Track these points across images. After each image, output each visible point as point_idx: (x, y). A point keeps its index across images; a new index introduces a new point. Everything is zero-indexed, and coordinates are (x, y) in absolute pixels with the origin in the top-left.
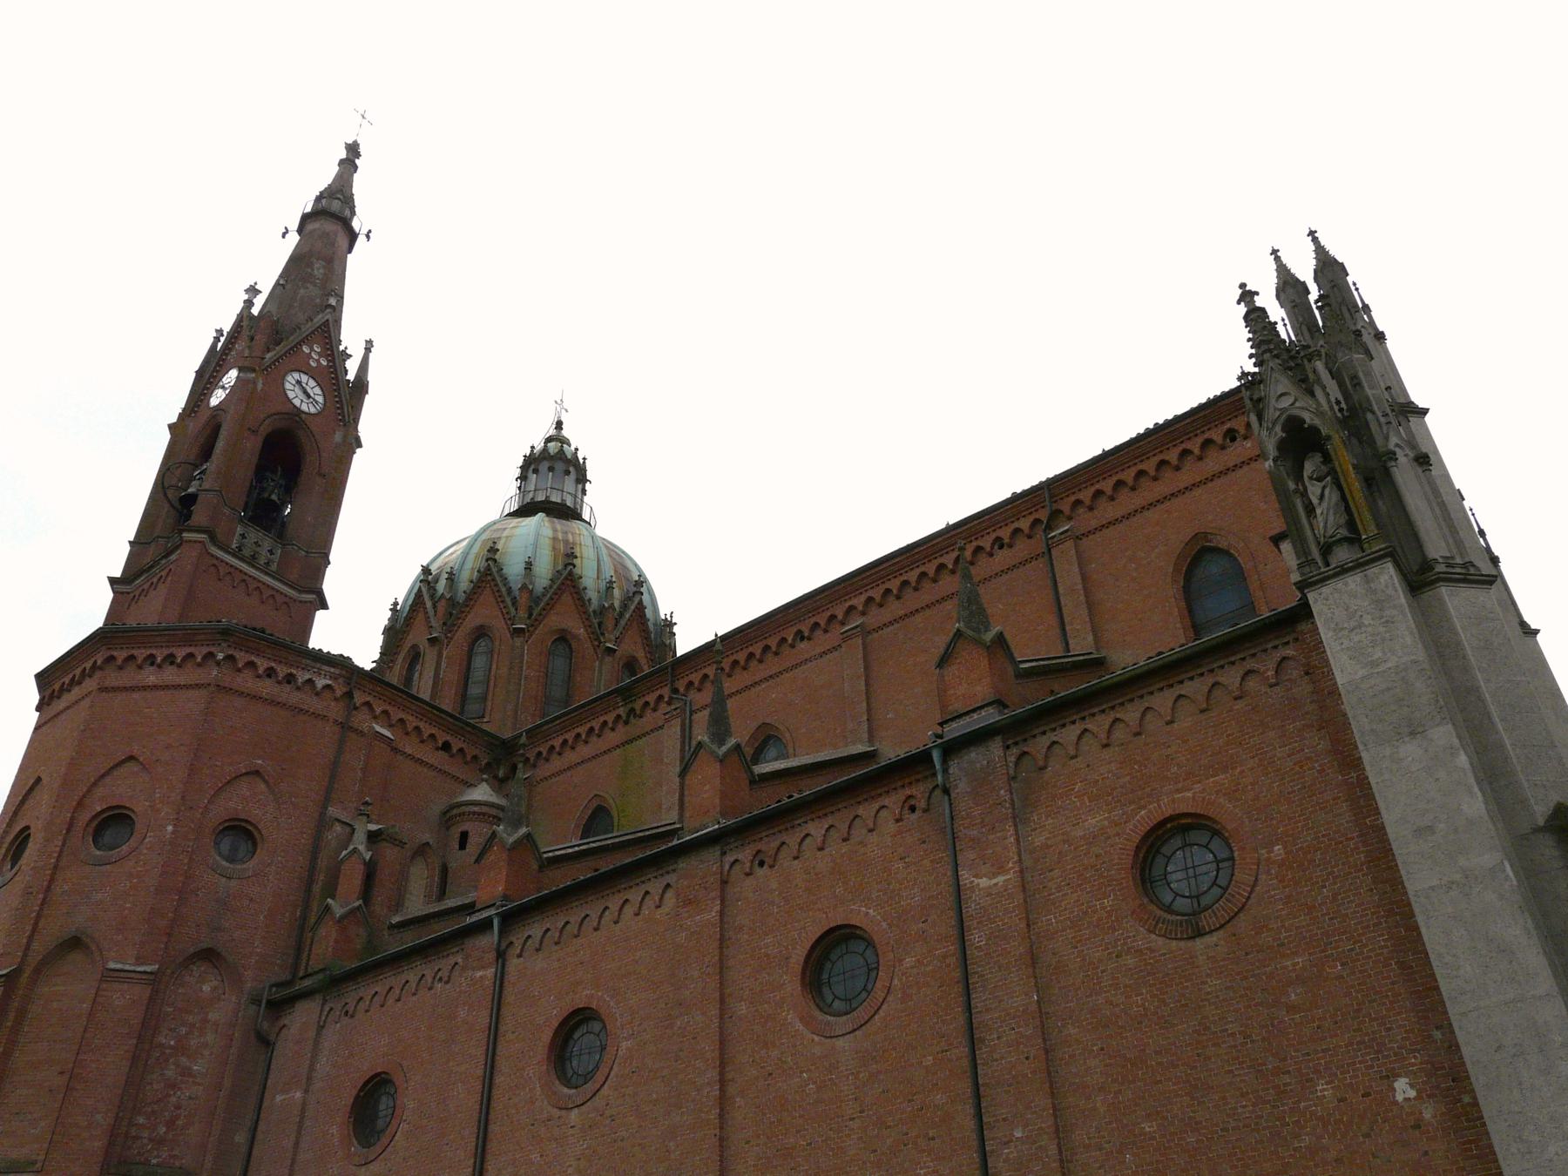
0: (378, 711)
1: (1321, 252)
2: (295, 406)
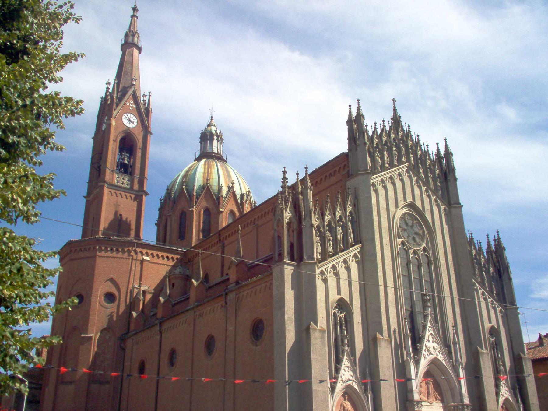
0: (144, 252)
2: (127, 127)
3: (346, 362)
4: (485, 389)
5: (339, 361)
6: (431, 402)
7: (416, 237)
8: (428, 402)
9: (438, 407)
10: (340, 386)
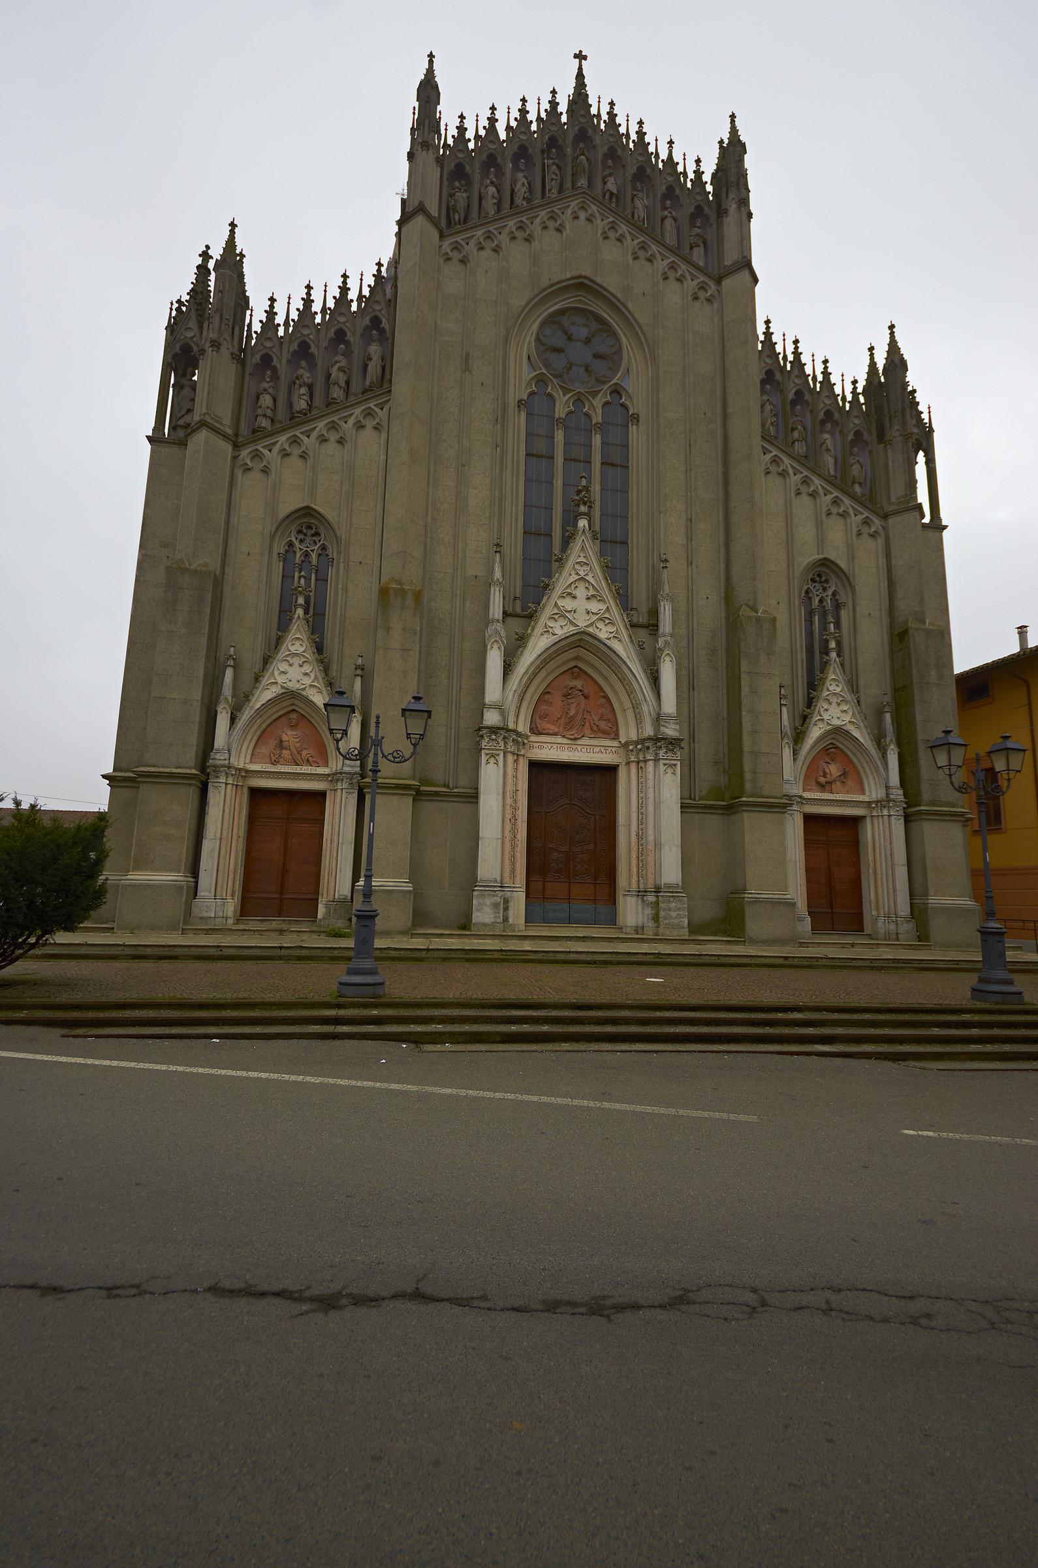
3: (834, 684)
5: (813, 685)
6: (572, 737)
8: (564, 736)
9: (596, 749)
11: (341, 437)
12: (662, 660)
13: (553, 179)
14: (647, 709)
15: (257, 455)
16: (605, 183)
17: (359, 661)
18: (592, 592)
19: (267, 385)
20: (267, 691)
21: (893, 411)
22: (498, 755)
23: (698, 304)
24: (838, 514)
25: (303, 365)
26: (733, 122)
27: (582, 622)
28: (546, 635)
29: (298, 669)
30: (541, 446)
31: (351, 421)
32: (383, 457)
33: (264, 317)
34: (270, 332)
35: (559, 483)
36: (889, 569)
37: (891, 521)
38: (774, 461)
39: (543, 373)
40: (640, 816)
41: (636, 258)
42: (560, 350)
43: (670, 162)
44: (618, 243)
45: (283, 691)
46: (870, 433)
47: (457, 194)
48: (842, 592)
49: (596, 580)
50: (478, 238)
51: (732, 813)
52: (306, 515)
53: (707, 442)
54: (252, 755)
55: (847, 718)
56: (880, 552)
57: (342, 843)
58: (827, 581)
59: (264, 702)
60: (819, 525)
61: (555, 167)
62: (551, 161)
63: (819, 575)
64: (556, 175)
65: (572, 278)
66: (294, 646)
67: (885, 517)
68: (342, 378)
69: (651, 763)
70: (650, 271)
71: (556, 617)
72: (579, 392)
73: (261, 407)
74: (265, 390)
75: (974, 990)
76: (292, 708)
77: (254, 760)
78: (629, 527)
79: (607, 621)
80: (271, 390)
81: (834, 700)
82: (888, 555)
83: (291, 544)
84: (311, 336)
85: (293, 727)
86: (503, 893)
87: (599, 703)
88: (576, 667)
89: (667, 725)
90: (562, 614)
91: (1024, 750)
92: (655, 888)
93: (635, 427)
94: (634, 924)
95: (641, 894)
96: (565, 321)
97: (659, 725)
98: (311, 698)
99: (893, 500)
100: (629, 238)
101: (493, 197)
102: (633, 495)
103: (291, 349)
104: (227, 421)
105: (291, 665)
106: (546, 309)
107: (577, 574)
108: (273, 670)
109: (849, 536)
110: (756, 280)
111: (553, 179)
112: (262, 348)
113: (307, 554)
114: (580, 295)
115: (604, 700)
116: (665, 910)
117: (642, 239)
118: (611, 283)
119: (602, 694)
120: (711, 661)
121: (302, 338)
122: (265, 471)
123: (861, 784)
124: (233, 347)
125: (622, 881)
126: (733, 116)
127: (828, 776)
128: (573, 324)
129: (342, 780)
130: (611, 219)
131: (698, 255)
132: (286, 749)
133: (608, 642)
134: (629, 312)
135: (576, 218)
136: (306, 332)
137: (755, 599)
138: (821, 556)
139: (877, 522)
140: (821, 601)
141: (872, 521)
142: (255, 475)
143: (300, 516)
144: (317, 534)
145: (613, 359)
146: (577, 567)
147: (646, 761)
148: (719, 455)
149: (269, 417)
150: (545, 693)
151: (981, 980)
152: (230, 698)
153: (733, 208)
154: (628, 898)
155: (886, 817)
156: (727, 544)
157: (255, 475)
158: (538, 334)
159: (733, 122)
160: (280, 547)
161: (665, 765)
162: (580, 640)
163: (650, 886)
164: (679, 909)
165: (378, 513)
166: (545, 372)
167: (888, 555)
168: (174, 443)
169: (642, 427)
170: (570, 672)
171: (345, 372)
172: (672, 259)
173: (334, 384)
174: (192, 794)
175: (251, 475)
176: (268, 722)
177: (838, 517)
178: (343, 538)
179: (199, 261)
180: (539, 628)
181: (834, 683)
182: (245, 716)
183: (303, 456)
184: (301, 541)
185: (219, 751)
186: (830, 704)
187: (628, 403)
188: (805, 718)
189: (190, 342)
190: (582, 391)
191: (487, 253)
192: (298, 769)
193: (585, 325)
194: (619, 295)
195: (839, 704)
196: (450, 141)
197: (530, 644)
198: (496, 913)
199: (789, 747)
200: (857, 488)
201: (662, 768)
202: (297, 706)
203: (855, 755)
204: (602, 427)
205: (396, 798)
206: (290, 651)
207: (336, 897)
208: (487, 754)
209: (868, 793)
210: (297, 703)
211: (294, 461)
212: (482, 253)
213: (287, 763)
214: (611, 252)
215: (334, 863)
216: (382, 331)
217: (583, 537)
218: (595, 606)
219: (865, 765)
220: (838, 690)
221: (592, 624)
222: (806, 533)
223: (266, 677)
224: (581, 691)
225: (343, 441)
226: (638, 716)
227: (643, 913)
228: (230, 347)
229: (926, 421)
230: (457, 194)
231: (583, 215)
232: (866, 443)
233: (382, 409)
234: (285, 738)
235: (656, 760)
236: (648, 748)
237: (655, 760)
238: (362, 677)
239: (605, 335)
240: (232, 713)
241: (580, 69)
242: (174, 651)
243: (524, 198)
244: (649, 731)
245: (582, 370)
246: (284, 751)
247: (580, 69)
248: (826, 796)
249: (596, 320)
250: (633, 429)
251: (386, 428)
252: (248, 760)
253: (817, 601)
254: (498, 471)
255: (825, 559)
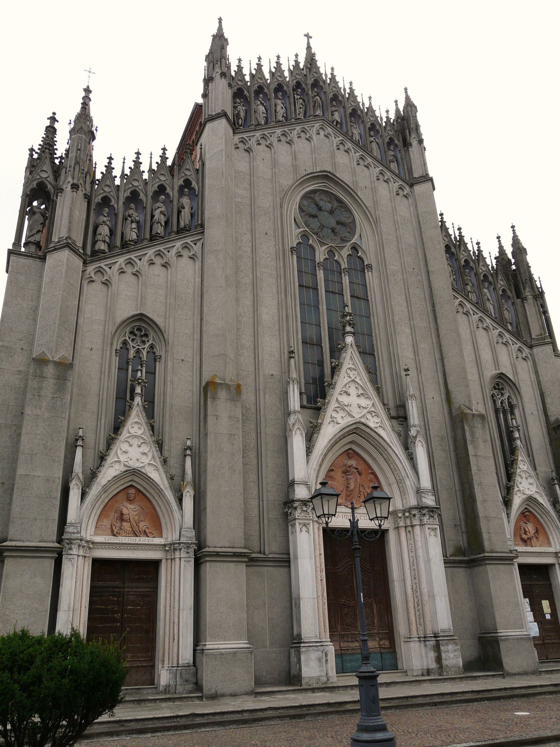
1: (408, 98)
4: (475, 478)
5: (117, 428)
7: (338, 227)
10: (517, 501)
11: (166, 262)
12: (294, 433)
13: (300, 108)
14: (409, 483)
15: (100, 271)
16: (333, 115)
17: (189, 443)
18: (361, 391)
19: (105, 219)
20: (110, 469)
21: (524, 279)
22: (308, 524)
23: (399, 198)
24: (502, 343)
25: (133, 207)
26: (406, 92)
27: (357, 415)
28: (332, 424)
29: (137, 449)
30: (308, 281)
31: (174, 251)
32: (198, 280)
33: (104, 170)
34: (108, 181)
35: (323, 307)
36: (539, 383)
37: (535, 350)
38: (460, 304)
39: (306, 230)
40: (412, 572)
41: (358, 164)
42: (314, 216)
43: (370, 109)
44: (346, 154)
45: (126, 469)
46: (511, 291)
47: (239, 107)
48: (513, 397)
49: (362, 382)
50: (257, 138)
51: (473, 566)
52: (141, 320)
53: (417, 287)
54: (96, 527)
55: (146, 460)
56: (531, 371)
57: (183, 610)
58: (502, 389)
59: (109, 478)
60: (493, 351)
61: (301, 100)
62: (299, 97)
63: (498, 385)
64: (303, 106)
65: (322, 172)
66: (133, 429)
67: (531, 347)
68: (163, 219)
69: (418, 528)
70: (368, 174)
71: (338, 409)
72: (332, 246)
73: (101, 234)
74: (104, 222)
75: (355, 740)
76: (130, 483)
77: (96, 533)
78: (374, 343)
79: (374, 414)
80: (108, 223)
81: (524, 475)
82: (536, 373)
83: (125, 343)
84: (140, 187)
85: (130, 501)
86: (323, 648)
87: (369, 478)
88: (350, 449)
89: (426, 496)
90: (342, 407)
91: (337, 495)
92: (433, 634)
93: (370, 273)
94: (420, 668)
95: (424, 639)
96: (317, 197)
97: (421, 497)
98: (149, 475)
99: (534, 336)
100: (353, 151)
101: (263, 113)
102: (374, 320)
103: (126, 195)
104: (80, 244)
105: (131, 446)
106: (304, 189)
107: (349, 377)
108: (117, 450)
109: (512, 359)
110: (434, 189)
111: (300, 108)
112: (102, 191)
113: (138, 351)
114: (325, 183)
115: (372, 476)
116: (445, 652)
117: (361, 153)
118: (344, 176)
119: (370, 471)
120: (442, 445)
121: (134, 188)
122: (106, 284)
123: (548, 539)
124: (85, 190)
125: (401, 627)
126: (406, 89)
127: (528, 533)
128: (322, 200)
129: (180, 549)
130: (341, 138)
131: (393, 166)
132: (126, 521)
133: (376, 430)
134: (359, 197)
135: (319, 134)
136: (136, 184)
137: (470, 401)
138: (498, 372)
139: (526, 350)
140: (138, 351)
141: (523, 349)
142: (97, 286)
143: (131, 322)
144: (146, 335)
145: (351, 227)
146: (349, 371)
147: (412, 526)
148: (427, 298)
149: (107, 243)
150: (331, 470)
151: (362, 729)
152: (81, 475)
153: (415, 143)
154: (412, 644)
155: (177, 560)
156: (442, 359)
157: (97, 286)
158: (299, 204)
159: (406, 92)
160: (117, 345)
161: (429, 529)
162: (356, 428)
163: (429, 633)
164: (455, 651)
165: (196, 322)
166: (307, 230)
167: (536, 373)
168: (31, 257)
169: (375, 273)
170: (346, 453)
171: (165, 215)
172: (381, 168)
173: (158, 223)
174: (49, 565)
175: (93, 285)
176: (110, 497)
177: (503, 345)
178: (170, 340)
179: (48, 123)
180: (327, 419)
181: (521, 463)
182: (94, 491)
183: (136, 274)
184: (133, 340)
185: (72, 525)
186: (522, 478)
187: (363, 257)
188: (102, 458)
189: (45, 181)
190: (333, 245)
191: (262, 147)
192: (137, 540)
193: (329, 202)
194: (350, 186)
195: (527, 479)
196: (233, 74)
197: (322, 431)
198: (320, 667)
199: (79, 489)
200: (510, 327)
201: (427, 531)
202: (134, 481)
203: (542, 517)
204: (348, 271)
205: (232, 565)
206: (130, 433)
207: (180, 662)
208: (300, 524)
209: (553, 546)
210: (136, 479)
211: (129, 277)
212: (259, 147)
213: (127, 535)
214: (342, 158)
215: (176, 628)
216: (192, 190)
217: (351, 350)
218: (364, 402)
219: (549, 524)
220: (140, 432)
221: (364, 416)
222: (486, 355)
223: (111, 456)
224: (356, 469)
225: (167, 265)
226: (402, 490)
227: (427, 657)
228: (84, 190)
229: (539, 286)
230: (239, 107)
231: (322, 133)
232: (509, 297)
233: (195, 244)
234: (125, 511)
235: (422, 525)
236: (414, 515)
237: (420, 525)
238: (191, 456)
239: (343, 210)
240: (82, 489)
241: (308, 43)
242: (39, 432)
243: (283, 116)
244: (413, 502)
245: (330, 231)
246: (124, 524)
247: (308, 43)
248: (529, 549)
249: (336, 200)
250: (368, 275)
251: (200, 259)
252: (92, 534)
253: (500, 403)
254: (283, 296)
255: (502, 373)
